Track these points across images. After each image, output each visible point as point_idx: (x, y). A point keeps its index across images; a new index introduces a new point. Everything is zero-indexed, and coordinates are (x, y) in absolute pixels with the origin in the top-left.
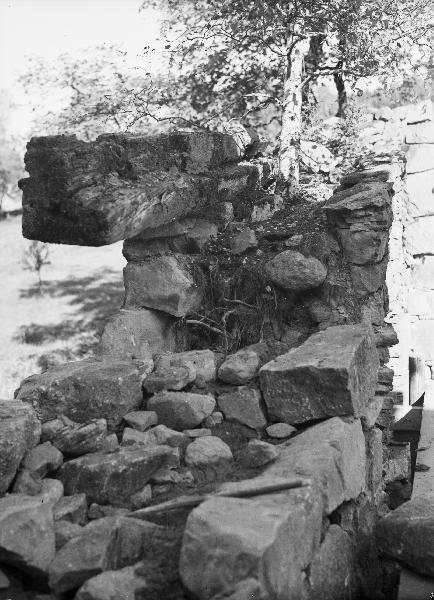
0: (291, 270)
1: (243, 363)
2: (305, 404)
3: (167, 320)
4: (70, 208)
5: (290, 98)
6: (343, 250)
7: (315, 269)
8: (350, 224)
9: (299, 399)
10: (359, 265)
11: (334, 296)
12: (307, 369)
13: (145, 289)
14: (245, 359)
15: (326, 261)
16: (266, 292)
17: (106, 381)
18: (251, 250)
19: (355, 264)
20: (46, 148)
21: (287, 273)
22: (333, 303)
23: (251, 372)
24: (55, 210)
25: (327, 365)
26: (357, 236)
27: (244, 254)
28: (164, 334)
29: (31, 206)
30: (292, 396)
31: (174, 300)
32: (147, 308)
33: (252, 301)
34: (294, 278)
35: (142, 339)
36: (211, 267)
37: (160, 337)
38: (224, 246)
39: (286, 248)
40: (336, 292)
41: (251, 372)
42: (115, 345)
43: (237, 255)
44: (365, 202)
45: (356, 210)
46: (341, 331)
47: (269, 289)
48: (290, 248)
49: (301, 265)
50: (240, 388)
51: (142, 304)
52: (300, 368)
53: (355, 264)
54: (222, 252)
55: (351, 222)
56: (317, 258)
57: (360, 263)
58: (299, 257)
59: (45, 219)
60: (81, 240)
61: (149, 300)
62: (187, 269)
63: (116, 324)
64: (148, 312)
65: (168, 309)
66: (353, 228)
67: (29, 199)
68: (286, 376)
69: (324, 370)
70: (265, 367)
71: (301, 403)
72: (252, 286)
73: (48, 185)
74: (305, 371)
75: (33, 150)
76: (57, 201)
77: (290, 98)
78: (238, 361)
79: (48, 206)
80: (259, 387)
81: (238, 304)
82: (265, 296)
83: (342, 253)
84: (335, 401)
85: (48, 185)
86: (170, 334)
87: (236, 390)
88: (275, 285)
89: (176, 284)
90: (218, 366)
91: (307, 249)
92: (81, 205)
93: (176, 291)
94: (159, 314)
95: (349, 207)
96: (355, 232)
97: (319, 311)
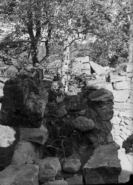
0: (84, 124)
1: (74, 164)
2: (100, 180)
3: (37, 145)
4: (25, 112)
5: (66, 57)
6: (99, 115)
7: (91, 123)
8: (102, 106)
9: (98, 178)
10: (105, 121)
11: (99, 133)
12: (104, 167)
13: (28, 134)
14: (75, 162)
15: (93, 120)
16: (74, 132)
17: (28, 181)
18: (65, 116)
19: (103, 120)
20: (14, 85)
21: (82, 125)
22: (99, 136)
23: (20, 145)
24: (18, 112)
25: (112, 166)
26: (104, 111)
27: (63, 117)
28: (35, 151)
29: (6, 111)
30: (95, 177)
31: (41, 138)
32: (29, 141)
33: (69, 136)
34: (85, 127)
35: (28, 154)
36: (52, 123)
37: (34, 153)
38: (53, 114)
39: (79, 115)
40: (99, 131)
41: (20, 145)
42: (19, 159)
43: (60, 118)
44: (109, 99)
45: (106, 101)
46: (106, 148)
47: (75, 131)
48: (81, 115)
49: (87, 122)
50: (75, 175)
51: (27, 140)
52: (101, 167)
53: (103, 120)
54: (54, 116)
55: (96, 103)
56: (91, 119)
57: (106, 120)
58: (86, 119)
59: (13, 117)
60: (29, 126)
61: (30, 138)
62: (44, 125)
63: (19, 150)
64: (29, 143)
65: (39, 142)
66: (103, 108)
67: (5, 108)
68: (95, 170)
69: (111, 168)
70: (85, 167)
71: (99, 180)
72: (69, 130)
73: (15, 102)
74: (103, 168)
75: (8, 86)
76: (19, 109)
77: (66, 57)
78: (72, 163)
79: (14, 111)
80: (82, 174)
81: (64, 138)
82: (73, 134)
83: (98, 116)
84: (112, 178)
85: (15, 102)
86: (37, 150)
87: (73, 176)
88: (77, 129)
89: (42, 131)
90: (62, 165)
91: (88, 115)
92: (30, 110)
93: (42, 134)
94: (33, 143)
95: (102, 100)
96: (103, 109)
97: (93, 139)
